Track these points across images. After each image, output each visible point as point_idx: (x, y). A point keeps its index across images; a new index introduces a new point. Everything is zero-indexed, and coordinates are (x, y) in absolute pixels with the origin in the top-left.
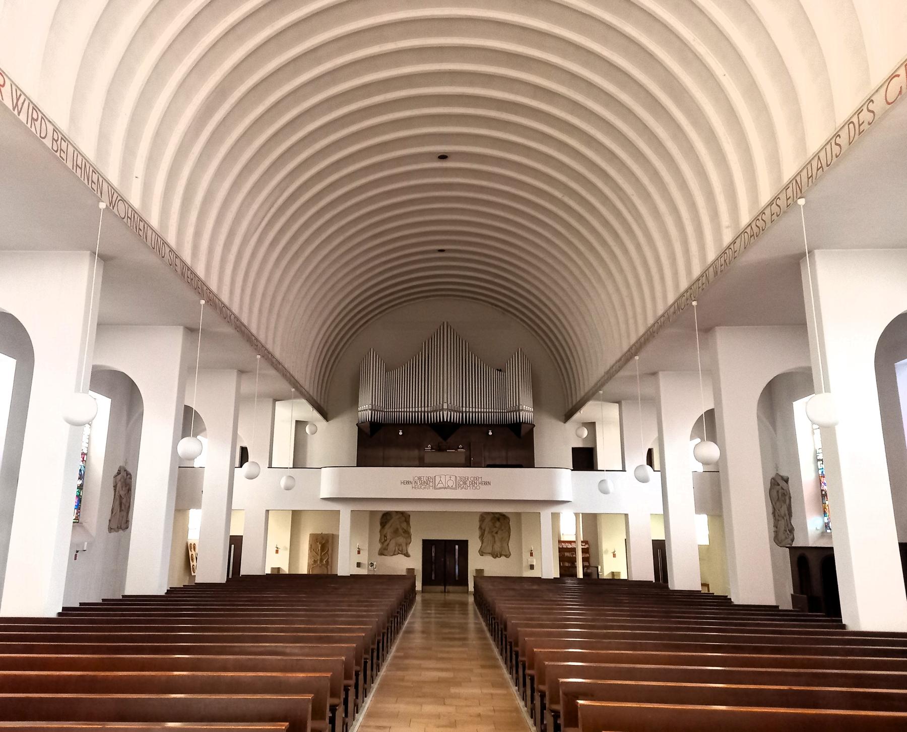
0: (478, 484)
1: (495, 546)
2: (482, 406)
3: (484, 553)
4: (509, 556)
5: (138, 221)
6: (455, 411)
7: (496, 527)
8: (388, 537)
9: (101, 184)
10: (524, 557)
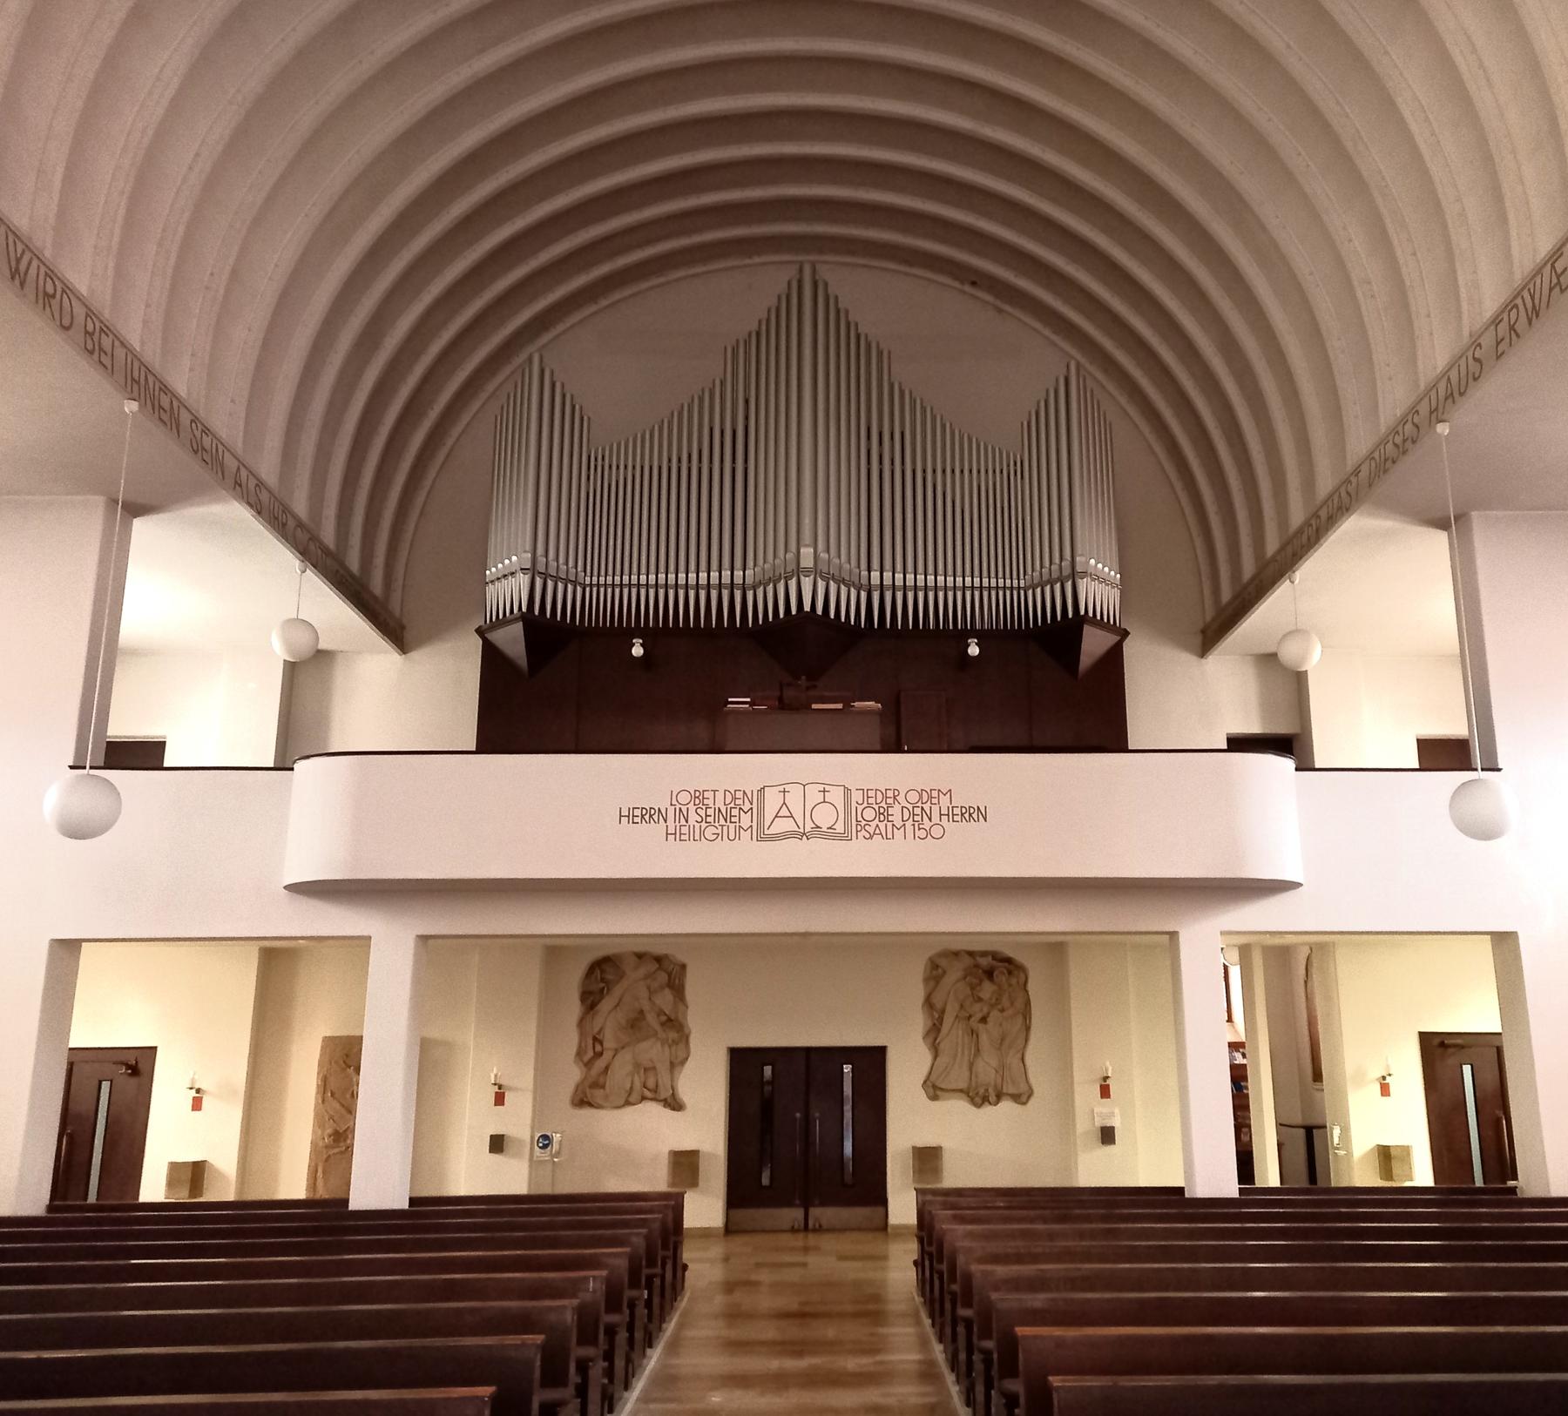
0: (936, 818)
1: (980, 1066)
3: (942, 1089)
4: (1029, 1097)
5: (157, 393)
6: (843, 581)
7: (980, 1000)
8: (609, 1043)
9: (176, 412)
10: (1077, 1098)
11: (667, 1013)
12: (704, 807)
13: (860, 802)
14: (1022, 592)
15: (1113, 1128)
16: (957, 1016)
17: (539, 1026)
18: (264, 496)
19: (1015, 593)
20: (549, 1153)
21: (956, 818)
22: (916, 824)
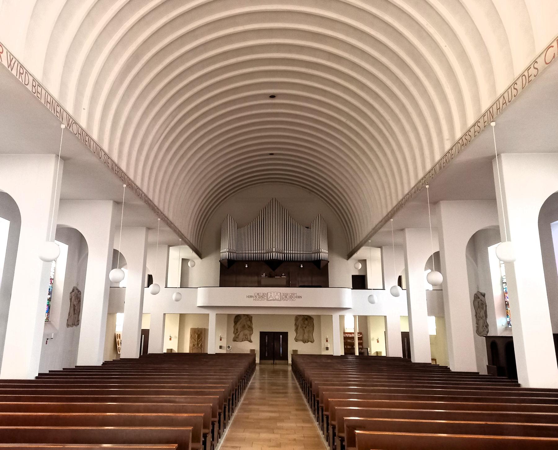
0: (294, 298)
1: (305, 336)
2: (297, 250)
3: (298, 340)
4: (313, 342)
5: (85, 136)
6: (280, 253)
7: (305, 324)
8: (239, 330)
9: (62, 113)
10: (322, 342)
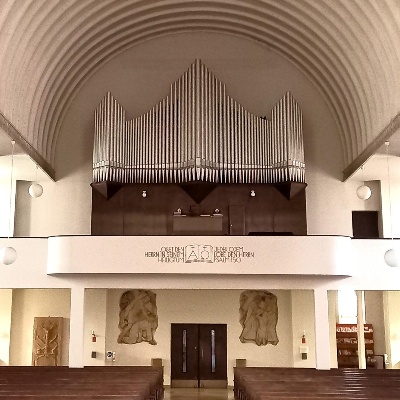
0: (238, 256)
1: (260, 331)
7: (260, 308)
8: (130, 321)
11: (150, 311)
12: (169, 252)
13: (216, 251)
14: (271, 170)
15: (306, 354)
16: (252, 314)
17: (106, 315)
18: (12, 130)
19: (269, 170)
20: (111, 359)
21: (244, 256)
22: (232, 258)
